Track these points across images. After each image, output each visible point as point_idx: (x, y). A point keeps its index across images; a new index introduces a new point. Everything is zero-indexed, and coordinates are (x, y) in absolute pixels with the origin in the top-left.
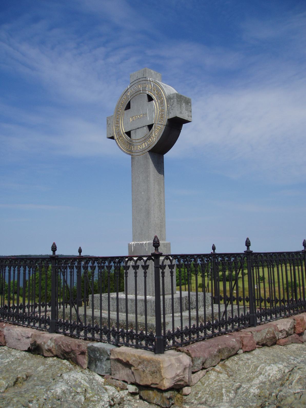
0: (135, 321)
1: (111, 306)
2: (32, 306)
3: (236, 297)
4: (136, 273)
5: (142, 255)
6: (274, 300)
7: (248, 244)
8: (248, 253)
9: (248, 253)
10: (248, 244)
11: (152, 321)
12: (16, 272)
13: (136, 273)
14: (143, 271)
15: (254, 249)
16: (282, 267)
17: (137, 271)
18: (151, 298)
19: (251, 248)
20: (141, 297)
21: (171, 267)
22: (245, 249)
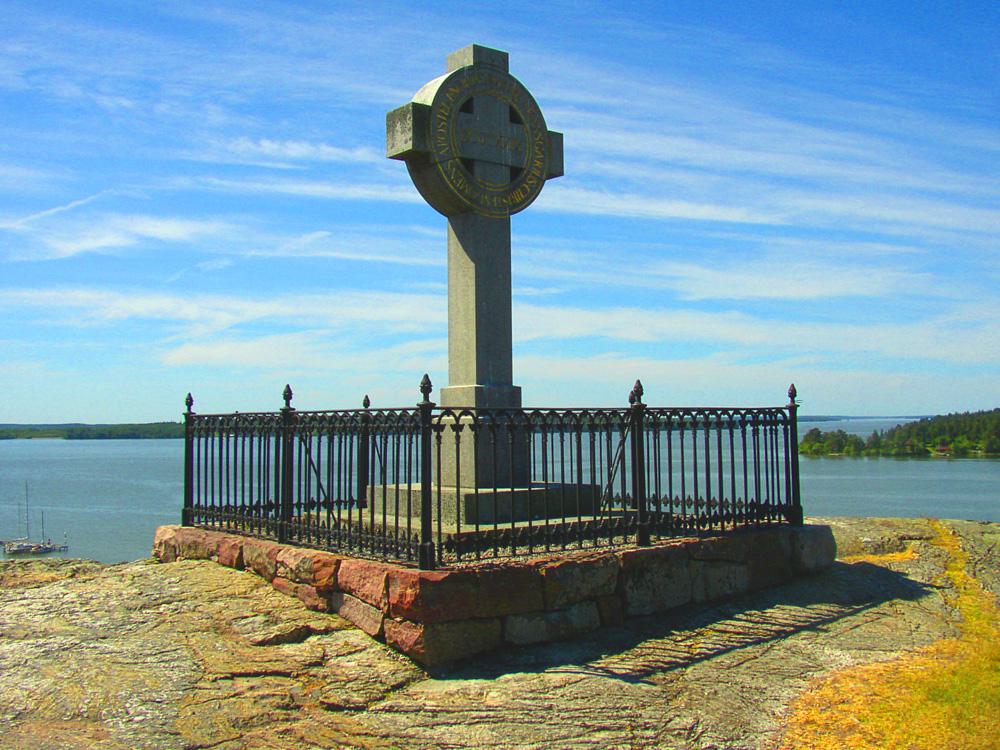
0: (394, 525)
1: (394, 500)
2: (264, 507)
3: (322, 508)
4: (458, 438)
5: (452, 406)
6: (530, 490)
7: (288, 395)
8: (288, 414)
9: (288, 414)
10: (288, 395)
11: (417, 524)
12: (348, 440)
13: (458, 438)
14: (455, 433)
15: (299, 404)
16: (417, 438)
17: (460, 433)
18: (417, 486)
19: (193, 409)
20: (403, 486)
21: (457, 428)
22: (420, 399)
